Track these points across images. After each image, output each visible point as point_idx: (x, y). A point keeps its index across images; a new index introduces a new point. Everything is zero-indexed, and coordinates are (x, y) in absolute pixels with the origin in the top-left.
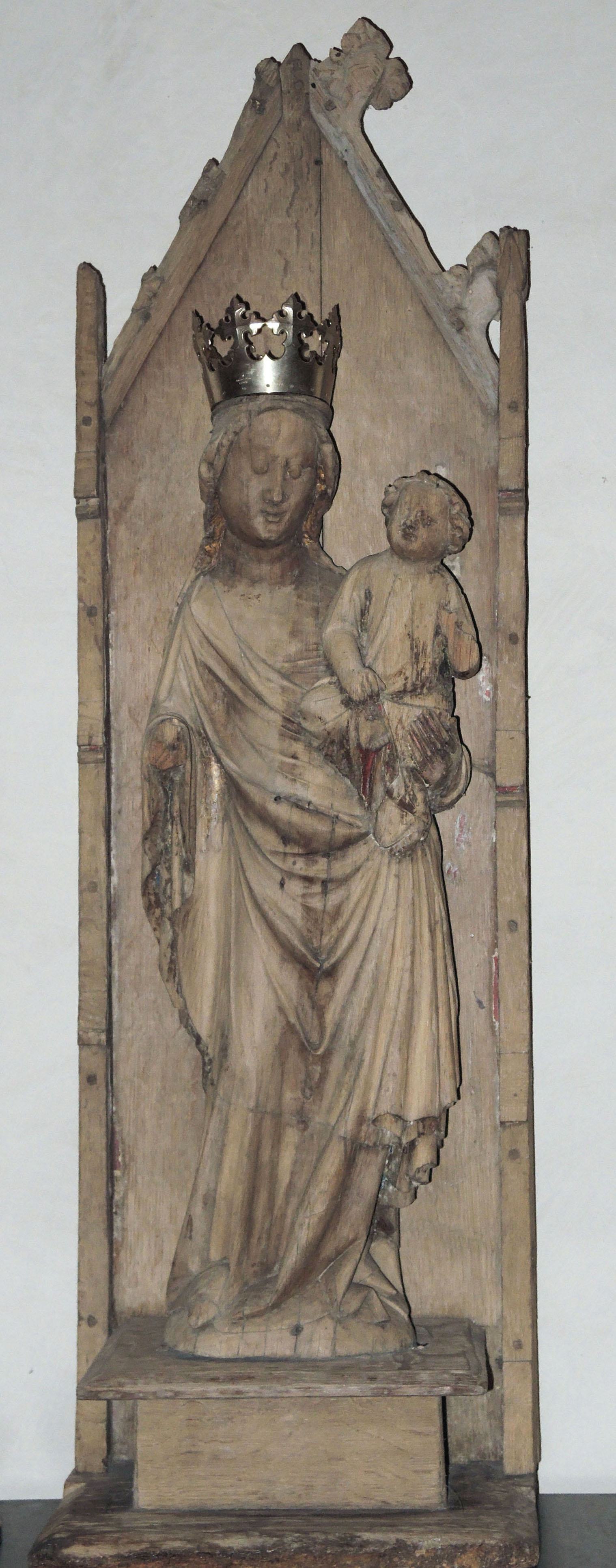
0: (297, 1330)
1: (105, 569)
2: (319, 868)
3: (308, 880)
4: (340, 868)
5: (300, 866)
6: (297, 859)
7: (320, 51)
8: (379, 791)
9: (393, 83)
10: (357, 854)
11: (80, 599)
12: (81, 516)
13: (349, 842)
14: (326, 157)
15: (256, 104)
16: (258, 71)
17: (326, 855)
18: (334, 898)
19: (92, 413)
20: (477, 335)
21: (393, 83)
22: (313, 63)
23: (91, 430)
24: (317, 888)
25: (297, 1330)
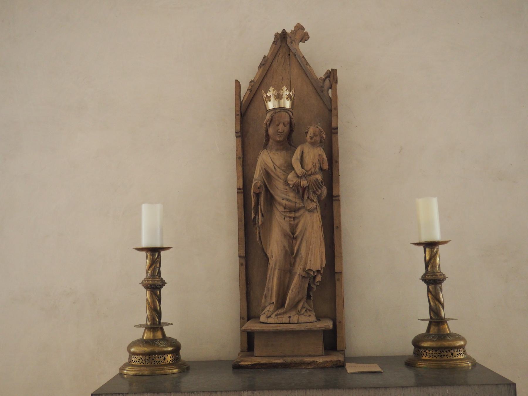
0: (290, 317)
1: (266, 74)
2: (293, 215)
3: (290, 217)
4: (297, 214)
5: (288, 215)
6: (288, 126)
7: (288, 31)
8: (306, 197)
9: (305, 37)
10: (302, 211)
11: (237, 155)
12: (237, 137)
13: (299, 209)
14: (291, 54)
15: (275, 43)
16: (275, 35)
17: (294, 212)
18: (296, 221)
19: (239, 113)
20: (325, 93)
21: (305, 37)
22: (269, 319)
23: (239, 117)
24: (292, 219)
25: (290, 317)
